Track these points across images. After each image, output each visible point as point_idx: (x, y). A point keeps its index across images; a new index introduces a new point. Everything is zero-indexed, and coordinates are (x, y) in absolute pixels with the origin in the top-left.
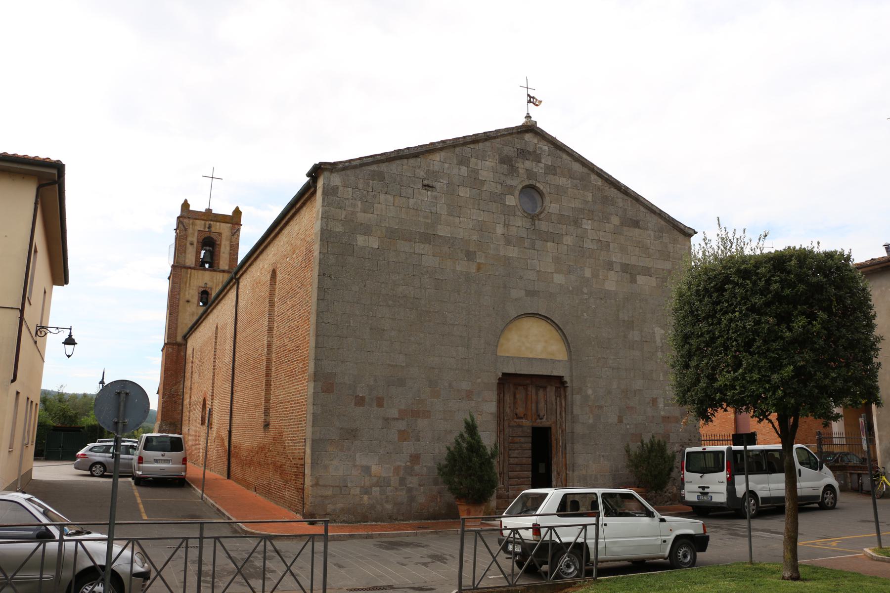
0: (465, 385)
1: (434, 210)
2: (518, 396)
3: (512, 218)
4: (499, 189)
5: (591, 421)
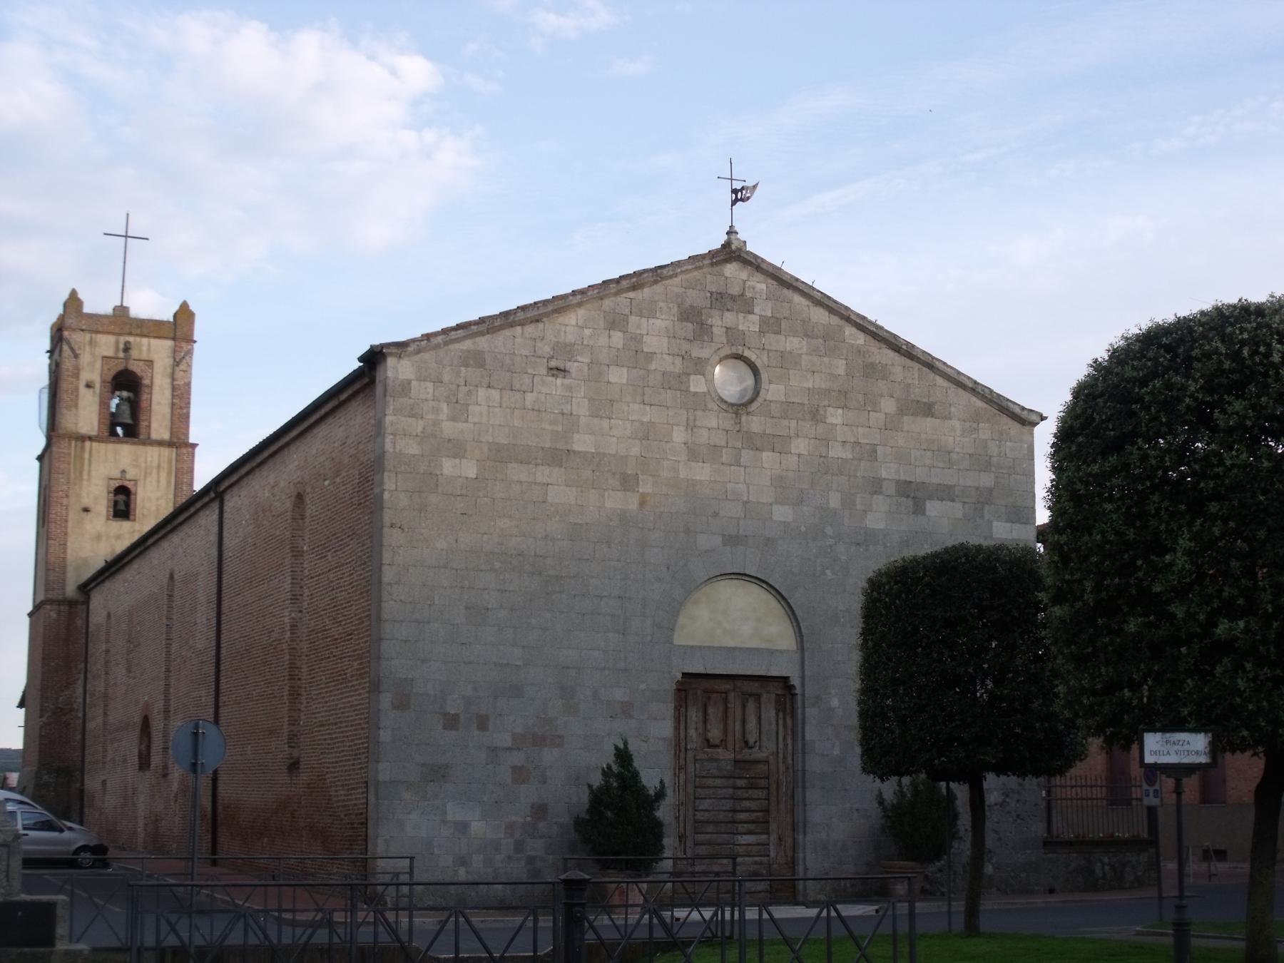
0: (619, 694)
1: (567, 409)
2: (710, 711)
3: (699, 413)
4: (678, 366)
5: (836, 752)
